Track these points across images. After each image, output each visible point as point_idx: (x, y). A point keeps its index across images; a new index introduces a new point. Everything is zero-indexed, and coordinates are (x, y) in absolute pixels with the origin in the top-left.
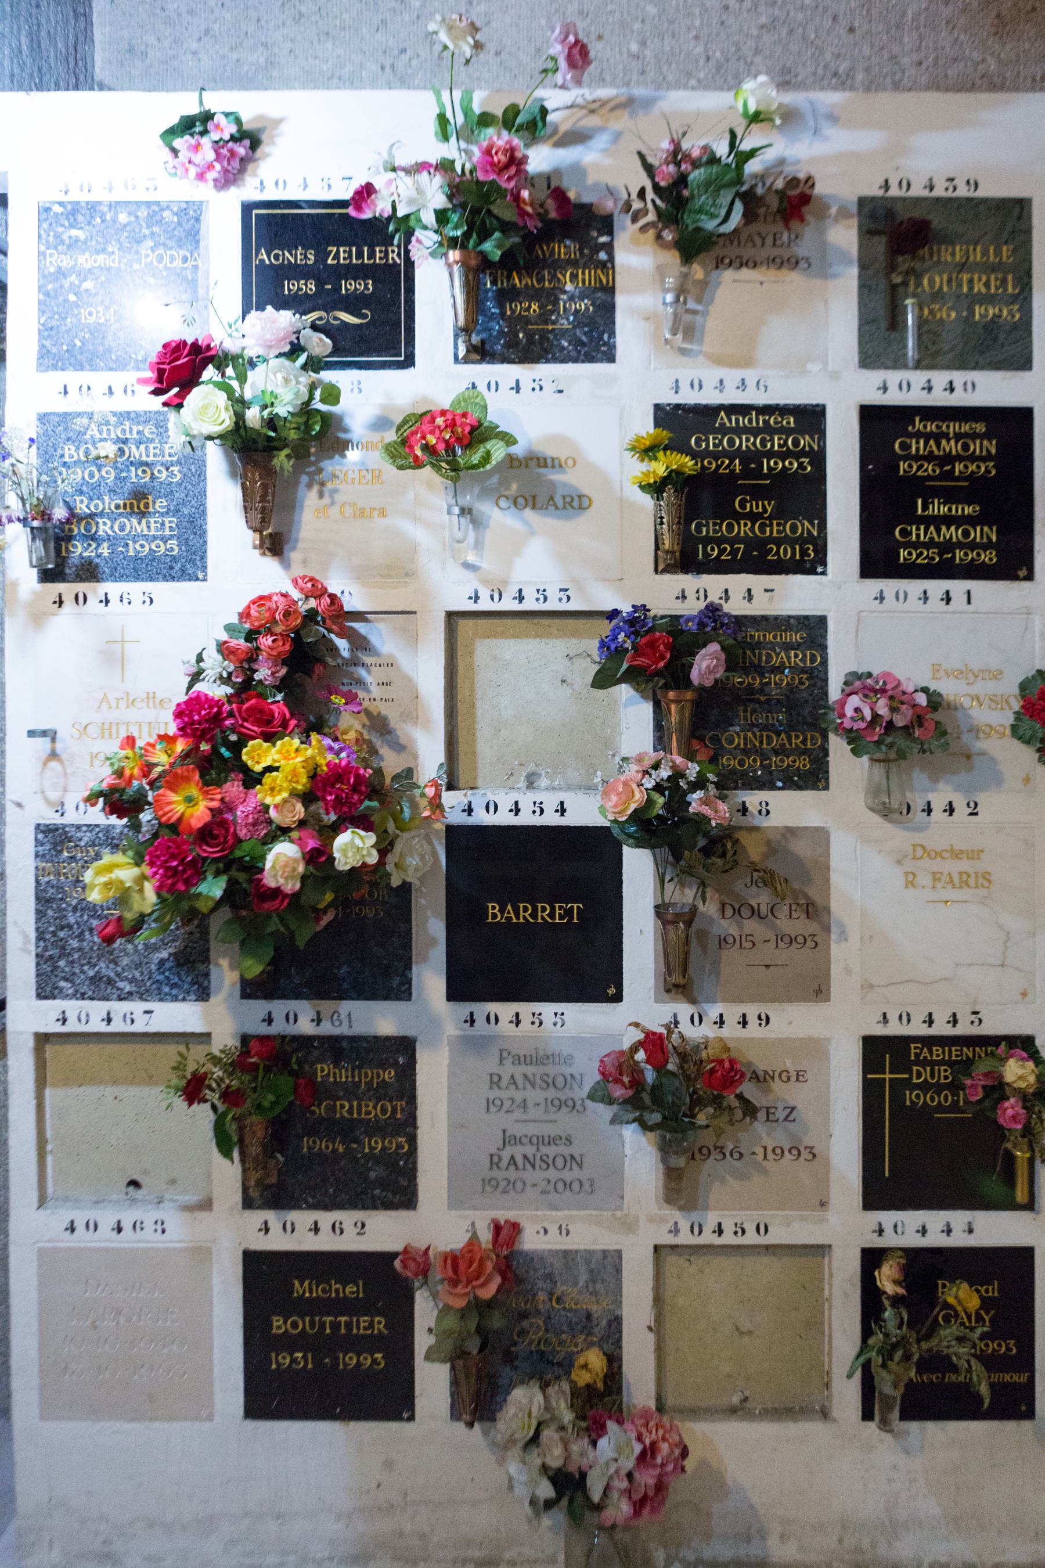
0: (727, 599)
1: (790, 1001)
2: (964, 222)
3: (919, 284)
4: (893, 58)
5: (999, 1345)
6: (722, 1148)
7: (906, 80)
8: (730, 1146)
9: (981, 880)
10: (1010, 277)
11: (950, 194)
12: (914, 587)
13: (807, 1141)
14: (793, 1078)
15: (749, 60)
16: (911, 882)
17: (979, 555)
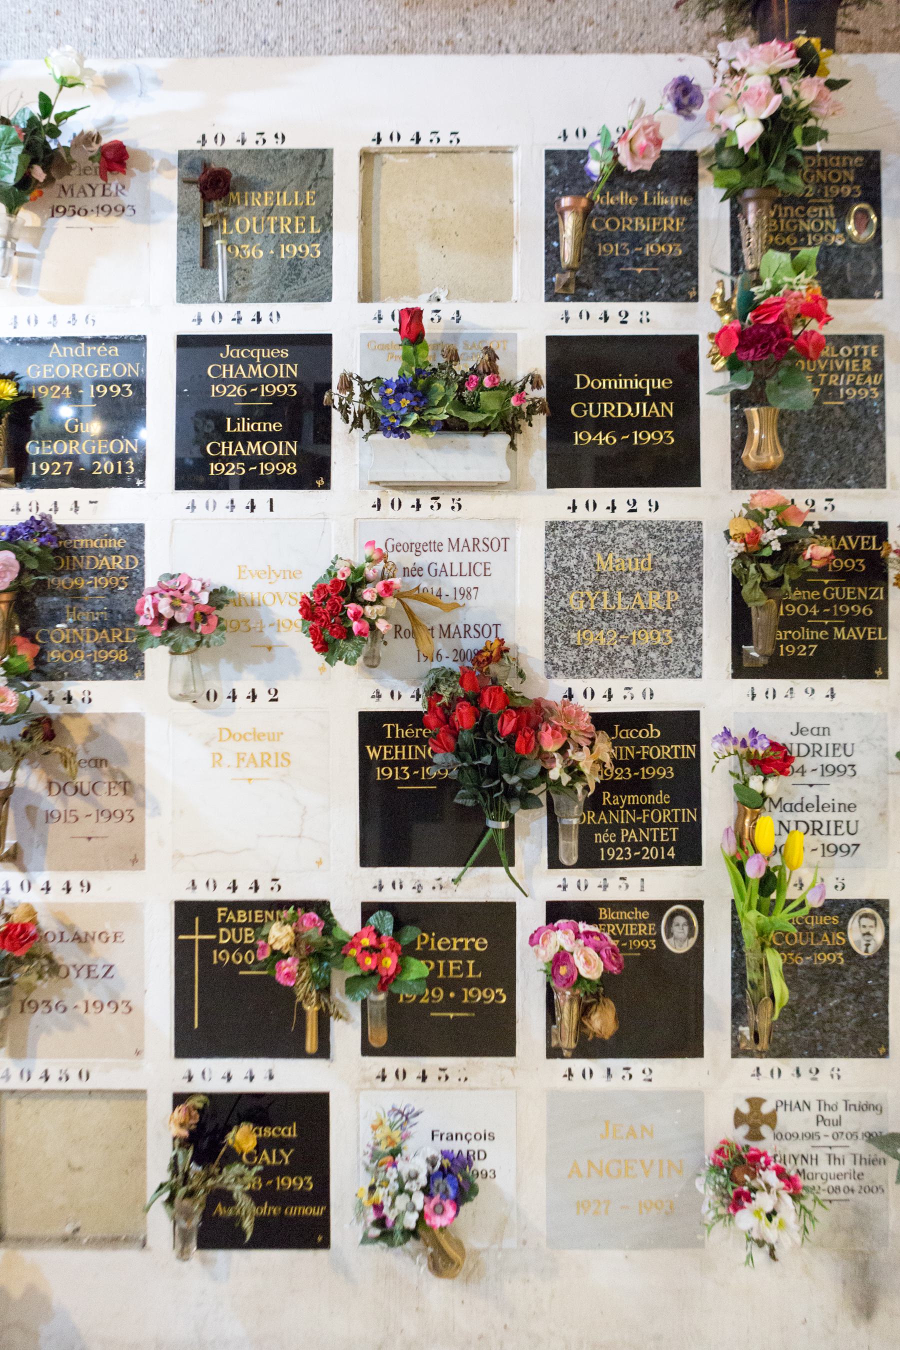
0: (56, 510)
1: (108, 869)
2: (272, 171)
3: (231, 226)
4: (316, 27)
5: (298, 1181)
6: (49, 1002)
7: (326, 46)
8: (55, 1000)
9: (280, 760)
10: (312, 218)
11: (260, 146)
12: (222, 496)
13: (124, 996)
14: (112, 939)
15: (189, 31)
16: (217, 760)
17: (281, 467)
